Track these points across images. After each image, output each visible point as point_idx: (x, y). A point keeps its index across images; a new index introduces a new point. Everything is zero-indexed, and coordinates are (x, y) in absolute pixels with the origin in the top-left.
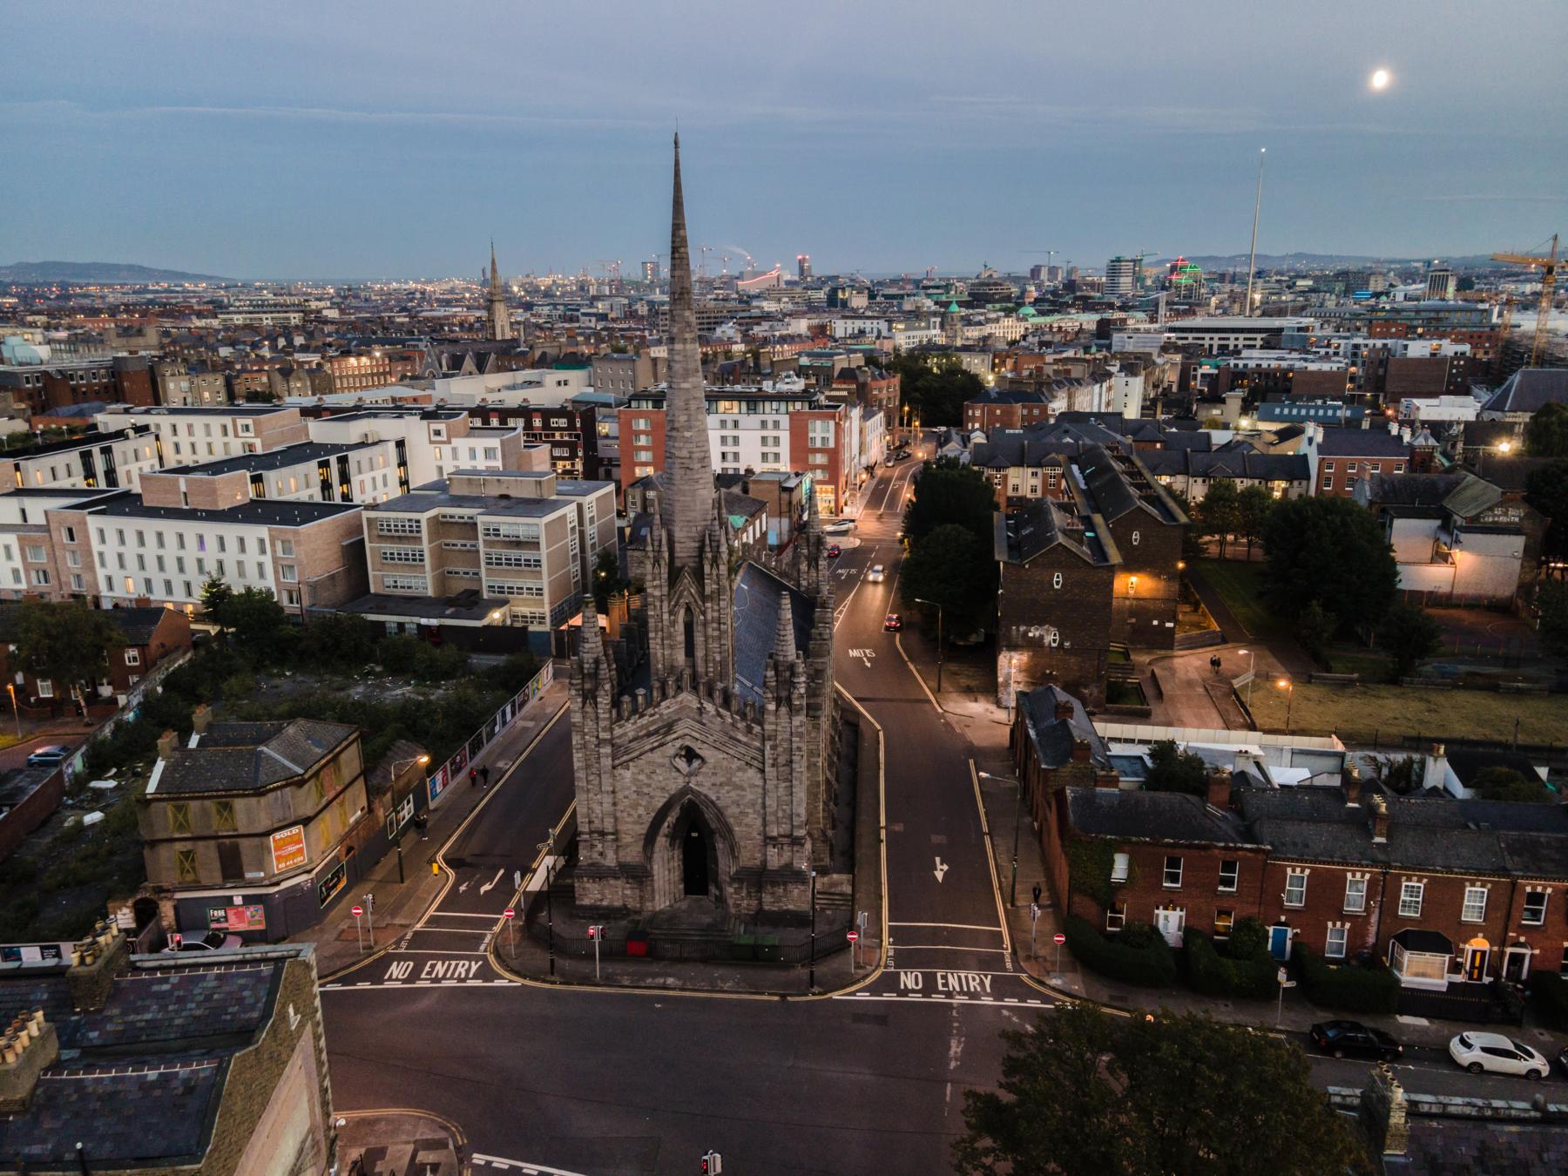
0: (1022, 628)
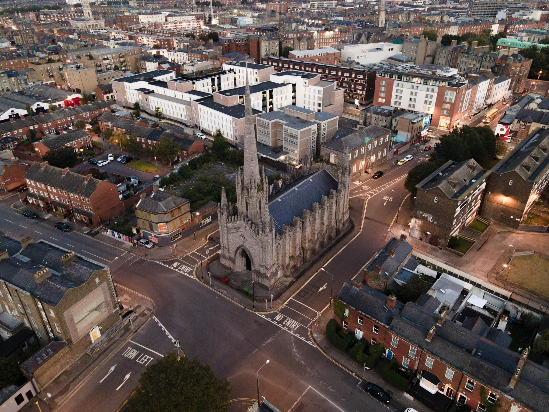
0: (421, 212)
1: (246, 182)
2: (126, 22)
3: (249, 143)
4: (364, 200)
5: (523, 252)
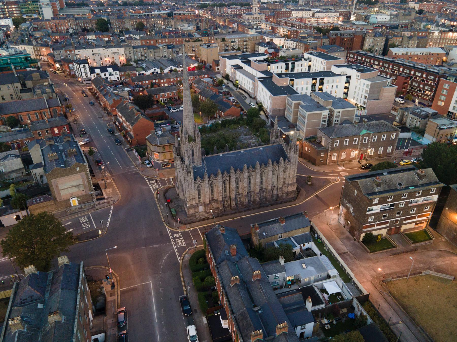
2: (281, 16)
5: (447, 276)
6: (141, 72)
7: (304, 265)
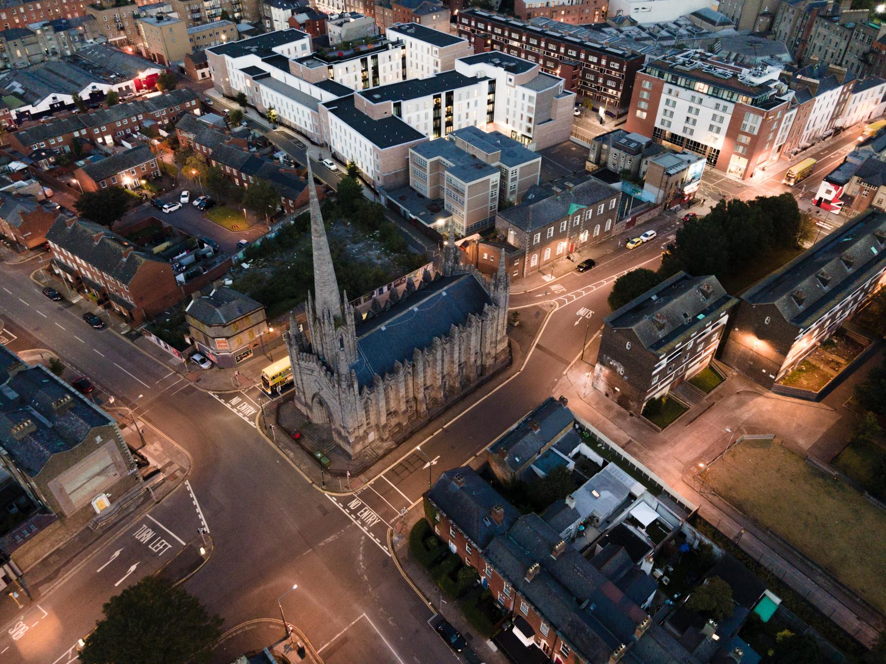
1: (319, 313)
3: (320, 262)
4: (546, 312)
6: (23, 109)
7: (595, 493)
